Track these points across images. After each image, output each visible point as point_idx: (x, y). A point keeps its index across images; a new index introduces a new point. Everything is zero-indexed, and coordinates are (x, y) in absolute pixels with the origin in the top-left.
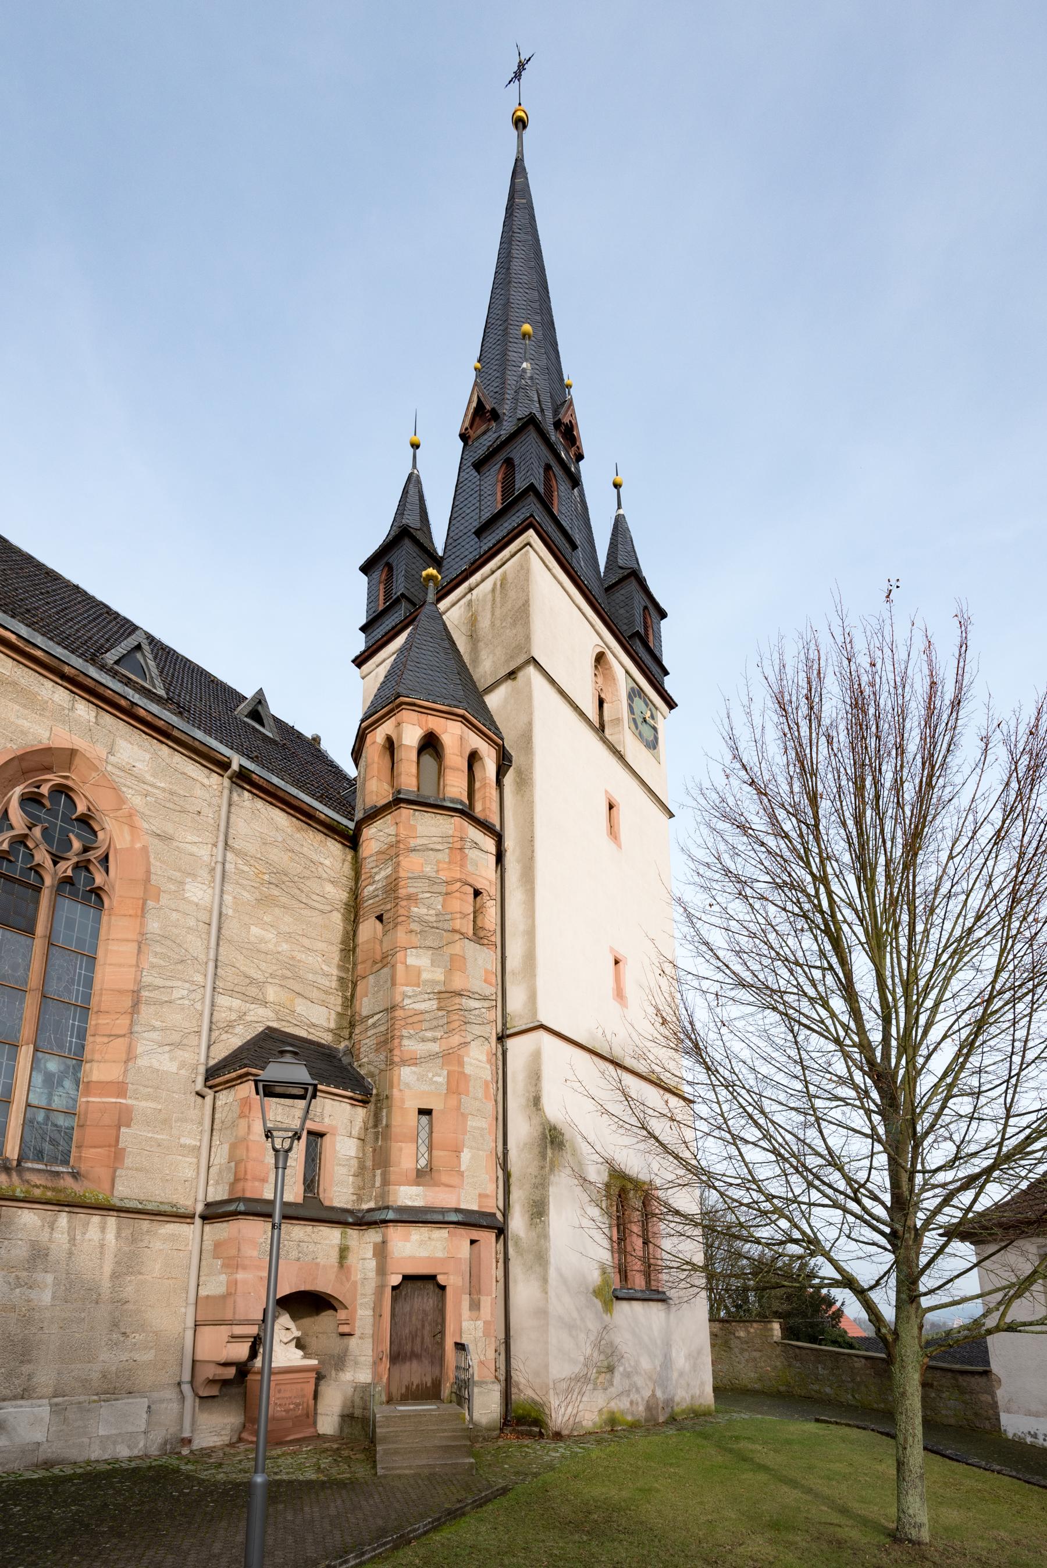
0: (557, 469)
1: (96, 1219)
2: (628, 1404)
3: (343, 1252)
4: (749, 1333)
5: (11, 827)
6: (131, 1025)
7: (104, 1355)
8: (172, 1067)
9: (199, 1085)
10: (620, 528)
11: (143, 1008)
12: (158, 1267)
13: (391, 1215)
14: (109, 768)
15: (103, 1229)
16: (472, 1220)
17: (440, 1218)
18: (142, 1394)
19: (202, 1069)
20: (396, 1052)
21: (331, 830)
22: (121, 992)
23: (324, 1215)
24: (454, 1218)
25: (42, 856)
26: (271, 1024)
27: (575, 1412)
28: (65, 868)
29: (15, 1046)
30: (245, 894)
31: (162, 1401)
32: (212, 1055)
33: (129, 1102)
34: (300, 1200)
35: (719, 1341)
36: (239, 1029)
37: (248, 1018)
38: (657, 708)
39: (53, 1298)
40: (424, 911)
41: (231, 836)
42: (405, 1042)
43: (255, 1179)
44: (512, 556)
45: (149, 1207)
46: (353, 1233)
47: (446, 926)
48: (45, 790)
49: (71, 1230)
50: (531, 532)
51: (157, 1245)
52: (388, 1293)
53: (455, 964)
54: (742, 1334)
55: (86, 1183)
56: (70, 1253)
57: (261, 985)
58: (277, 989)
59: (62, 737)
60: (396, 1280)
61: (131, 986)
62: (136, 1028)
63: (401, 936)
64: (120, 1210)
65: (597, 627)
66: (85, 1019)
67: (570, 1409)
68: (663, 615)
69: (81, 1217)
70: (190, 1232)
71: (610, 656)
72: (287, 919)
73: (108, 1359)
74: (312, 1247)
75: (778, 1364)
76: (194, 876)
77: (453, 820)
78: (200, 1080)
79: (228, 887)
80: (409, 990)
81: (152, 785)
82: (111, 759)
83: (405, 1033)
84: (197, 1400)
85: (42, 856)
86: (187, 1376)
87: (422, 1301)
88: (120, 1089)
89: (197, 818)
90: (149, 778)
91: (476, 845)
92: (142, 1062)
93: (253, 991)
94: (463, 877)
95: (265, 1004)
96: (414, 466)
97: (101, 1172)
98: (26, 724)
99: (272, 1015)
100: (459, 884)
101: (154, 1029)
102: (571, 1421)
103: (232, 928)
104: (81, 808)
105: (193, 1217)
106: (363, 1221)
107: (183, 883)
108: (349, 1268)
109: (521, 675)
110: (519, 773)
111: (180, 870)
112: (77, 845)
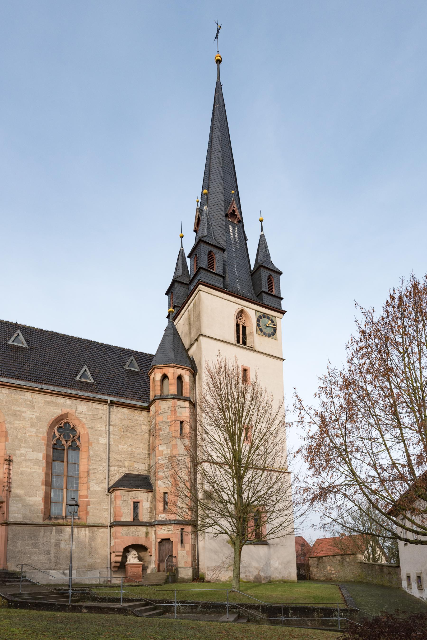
0: (214, 250)
1: (83, 529)
2: (244, 576)
3: (147, 534)
4: (350, 559)
5: (56, 436)
6: (88, 480)
7: (88, 560)
8: (99, 489)
9: (106, 493)
10: (262, 239)
11: (90, 475)
12: (100, 539)
13: (156, 523)
14: (76, 414)
15: (85, 531)
16: (180, 523)
17: (169, 523)
18: (98, 569)
19: (107, 488)
20: (157, 476)
21: (143, 408)
22: (85, 472)
23: (139, 524)
24: (173, 522)
25: (64, 442)
26: (127, 472)
27: (217, 576)
28: (69, 443)
29: (62, 490)
30: (116, 437)
31: (103, 571)
32: (110, 484)
33: (89, 499)
34: (132, 520)
35: (341, 563)
36: (117, 476)
37: (120, 472)
38: (276, 317)
39: (75, 547)
40: (163, 432)
41: (111, 421)
42: (159, 473)
43: (119, 516)
44: (196, 294)
45: (96, 525)
46: (150, 529)
47: (170, 436)
48: (62, 425)
49: (78, 531)
50: (200, 286)
51: (99, 534)
52: (157, 543)
53: (175, 447)
54: (348, 560)
55: (81, 520)
56: (78, 537)
57: (123, 462)
58: (128, 462)
59: (64, 410)
60: (159, 540)
61: (87, 470)
62: (89, 481)
63: (157, 441)
64: (89, 526)
65: (237, 302)
66: (78, 480)
67: (214, 575)
68: (280, 273)
69: (80, 528)
70: (108, 530)
71: (246, 309)
72: (130, 440)
73: (89, 561)
74: (137, 533)
75: (359, 570)
76: (101, 436)
77: (171, 401)
78: (107, 491)
79: (111, 436)
80: (160, 458)
81: (88, 415)
82: (77, 411)
83: (159, 470)
84: (112, 572)
85: (64, 442)
86: (109, 566)
87: (166, 546)
88: (87, 496)
89: (101, 419)
90: (87, 413)
91: (181, 407)
92: (91, 489)
93: (121, 464)
94: (176, 419)
95: (125, 467)
96: (182, 246)
97: (84, 517)
98: (56, 411)
99: (127, 469)
100: (174, 422)
101: (94, 480)
102: (215, 578)
103: (113, 448)
104: (72, 426)
105: (107, 526)
106: (151, 525)
107: (98, 439)
108: (149, 538)
109: (199, 339)
110: (199, 375)
111: (97, 436)
112: (72, 436)
